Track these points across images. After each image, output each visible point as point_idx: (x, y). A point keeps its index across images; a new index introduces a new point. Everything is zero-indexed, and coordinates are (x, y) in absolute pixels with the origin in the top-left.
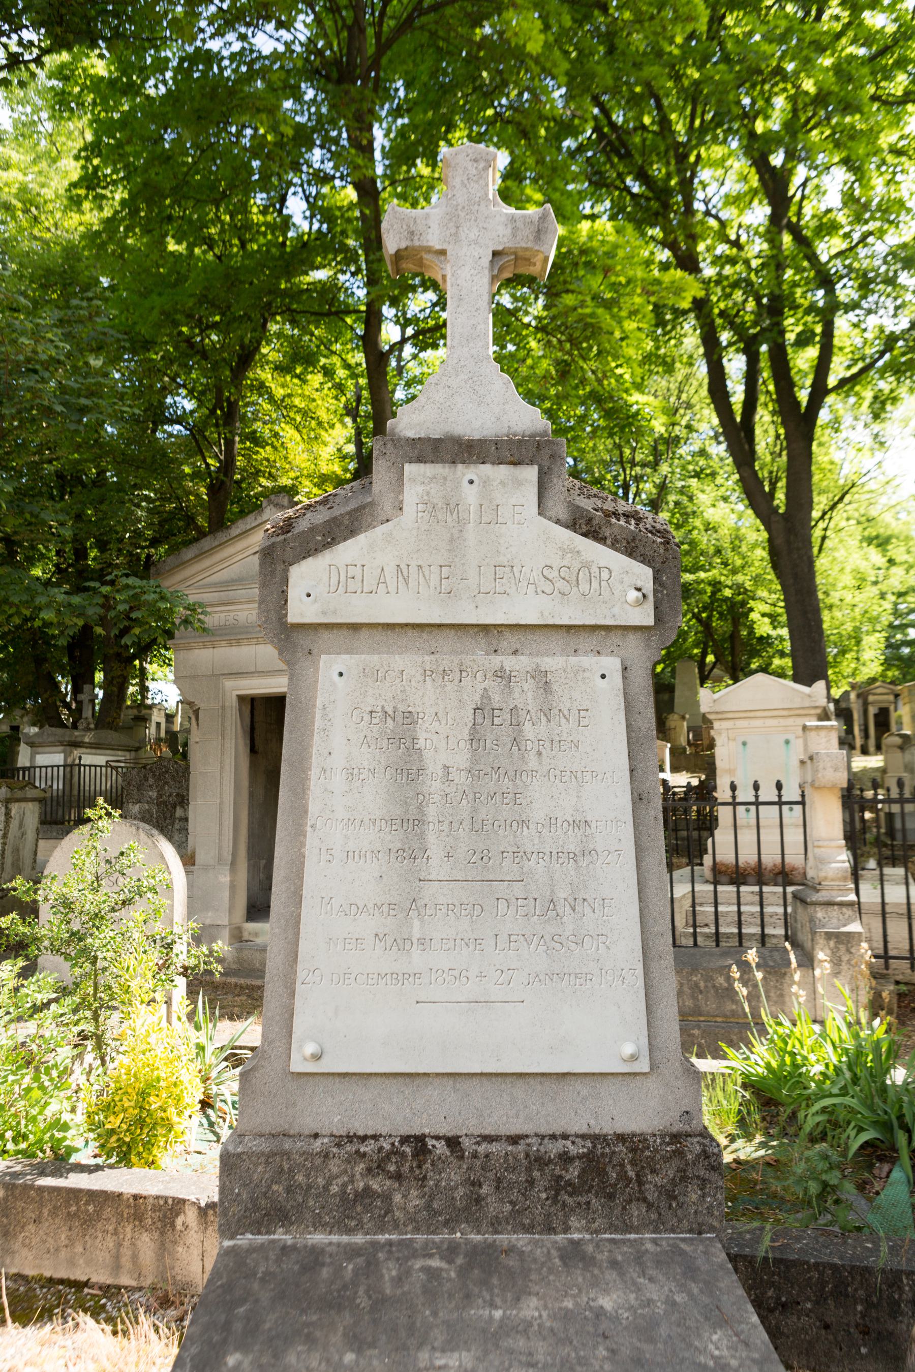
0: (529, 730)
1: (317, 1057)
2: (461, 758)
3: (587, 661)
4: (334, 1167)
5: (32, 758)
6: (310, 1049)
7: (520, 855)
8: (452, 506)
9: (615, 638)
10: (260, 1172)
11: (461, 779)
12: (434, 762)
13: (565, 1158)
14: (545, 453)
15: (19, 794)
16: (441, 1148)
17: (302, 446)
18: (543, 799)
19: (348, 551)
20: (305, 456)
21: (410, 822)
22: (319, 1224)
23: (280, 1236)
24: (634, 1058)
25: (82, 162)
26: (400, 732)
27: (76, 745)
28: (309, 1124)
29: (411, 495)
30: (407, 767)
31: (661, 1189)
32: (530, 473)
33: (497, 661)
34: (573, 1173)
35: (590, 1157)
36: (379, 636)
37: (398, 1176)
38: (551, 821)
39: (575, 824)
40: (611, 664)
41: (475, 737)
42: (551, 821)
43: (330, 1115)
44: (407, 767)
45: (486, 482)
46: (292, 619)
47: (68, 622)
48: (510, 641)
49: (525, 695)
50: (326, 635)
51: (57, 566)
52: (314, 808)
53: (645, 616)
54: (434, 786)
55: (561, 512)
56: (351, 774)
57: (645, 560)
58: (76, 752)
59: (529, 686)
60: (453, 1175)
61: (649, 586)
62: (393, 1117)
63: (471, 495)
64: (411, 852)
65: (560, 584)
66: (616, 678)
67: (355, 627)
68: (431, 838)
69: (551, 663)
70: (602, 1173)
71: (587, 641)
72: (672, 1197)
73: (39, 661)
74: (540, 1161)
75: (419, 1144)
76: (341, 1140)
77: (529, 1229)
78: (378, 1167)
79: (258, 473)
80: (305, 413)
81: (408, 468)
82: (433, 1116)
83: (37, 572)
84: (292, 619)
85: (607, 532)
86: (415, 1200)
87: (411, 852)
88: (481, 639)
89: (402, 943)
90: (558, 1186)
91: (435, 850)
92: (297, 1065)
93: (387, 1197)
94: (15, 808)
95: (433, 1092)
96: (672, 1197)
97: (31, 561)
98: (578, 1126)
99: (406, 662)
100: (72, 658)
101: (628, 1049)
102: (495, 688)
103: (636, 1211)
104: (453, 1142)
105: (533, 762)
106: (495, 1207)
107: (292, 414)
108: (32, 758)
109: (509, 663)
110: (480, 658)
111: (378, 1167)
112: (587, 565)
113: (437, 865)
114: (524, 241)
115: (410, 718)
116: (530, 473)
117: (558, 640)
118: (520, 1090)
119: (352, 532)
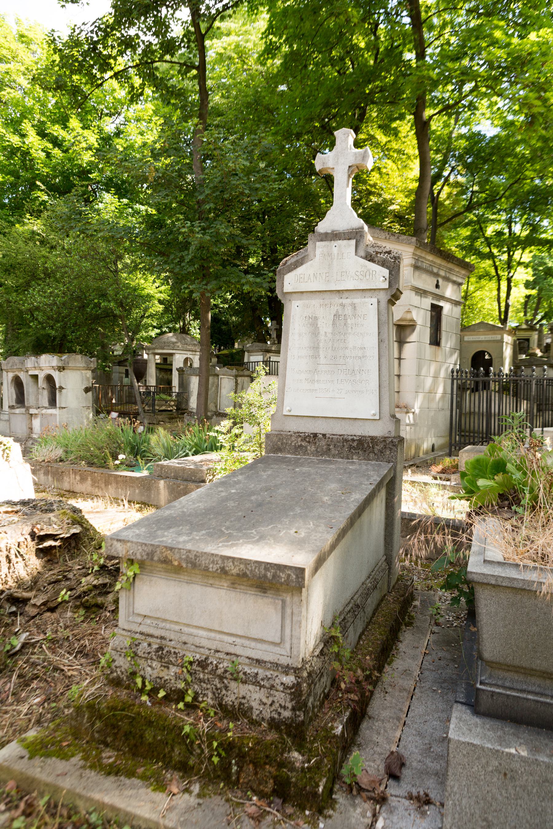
0: (349, 321)
1: (290, 411)
2: (330, 330)
3: (366, 300)
4: (293, 439)
5: (249, 358)
6: (288, 408)
7: (345, 357)
8: (330, 254)
9: (377, 292)
10: (275, 439)
11: (329, 336)
12: (322, 332)
13: (353, 440)
14: (359, 235)
15: (241, 373)
16: (320, 436)
17: (397, 173)
18: (352, 341)
19: (300, 270)
20: (399, 179)
21: (315, 348)
22: (289, 453)
23: (279, 455)
24: (374, 415)
25: (264, 40)
26: (313, 322)
27: (268, 351)
28: (288, 429)
29: (318, 252)
30: (315, 333)
31: (379, 450)
32: (353, 242)
33: (341, 300)
34: (355, 444)
35: (360, 440)
36: (309, 294)
37: (309, 442)
38: (354, 347)
39: (361, 348)
40: (374, 301)
41: (334, 324)
42: (354, 347)
43: (293, 426)
44: (315, 333)
45: (340, 246)
46: (285, 291)
47: (256, 290)
48: (346, 294)
49: (349, 311)
50: (294, 295)
51: (262, 257)
52: (290, 344)
53: (386, 285)
54: (322, 338)
55: (362, 254)
56: (300, 335)
57: (387, 268)
58: (268, 355)
59: (350, 308)
60: (323, 443)
61: (387, 276)
62: (309, 428)
63: (335, 251)
64: (315, 356)
65: (361, 277)
66: (375, 305)
67: (302, 292)
68: (321, 352)
69: (356, 301)
70: (363, 445)
71: (368, 294)
72: (382, 452)
73: (254, 309)
74: (346, 441)
75: (315, 435)
76: (295, 433)
77: (342, 458)
78: (304, 439)
79: (370, 193)
80: (399, 152)
81: (318, 244)
82: (320, 428)
83: (252, 261)
84: (285, 291)
85: (376, 259)
86: (313, 448)
87: (315, 356)
88: (337, 294)
89: (313, 381)
90: (351, 447)
91: (322, 356)
92: (285, 413)
93: (306, 447)
94: (240, 379)
95: (320, 422)
96: (382, 452)
97: (248, 256)
98: (359, 433)
99: (316, 302)
100: (270, 308)
101: (373, 412)
102: (339, 308)
103: (372, 455)
104: (324, 435)
105: (350, 330)
106: (334, 451)
107: (391, 153)
108: (249, 358)
109: (344, 301)
110: (337, 300)
111: (304, 439)
112: (369, 270)
113: (322, 360)
114: (358, 162)
115: (316, 318)
116: (353, 242)
117: (360, 293)
118: (343, 422)
119: (302, 264)
